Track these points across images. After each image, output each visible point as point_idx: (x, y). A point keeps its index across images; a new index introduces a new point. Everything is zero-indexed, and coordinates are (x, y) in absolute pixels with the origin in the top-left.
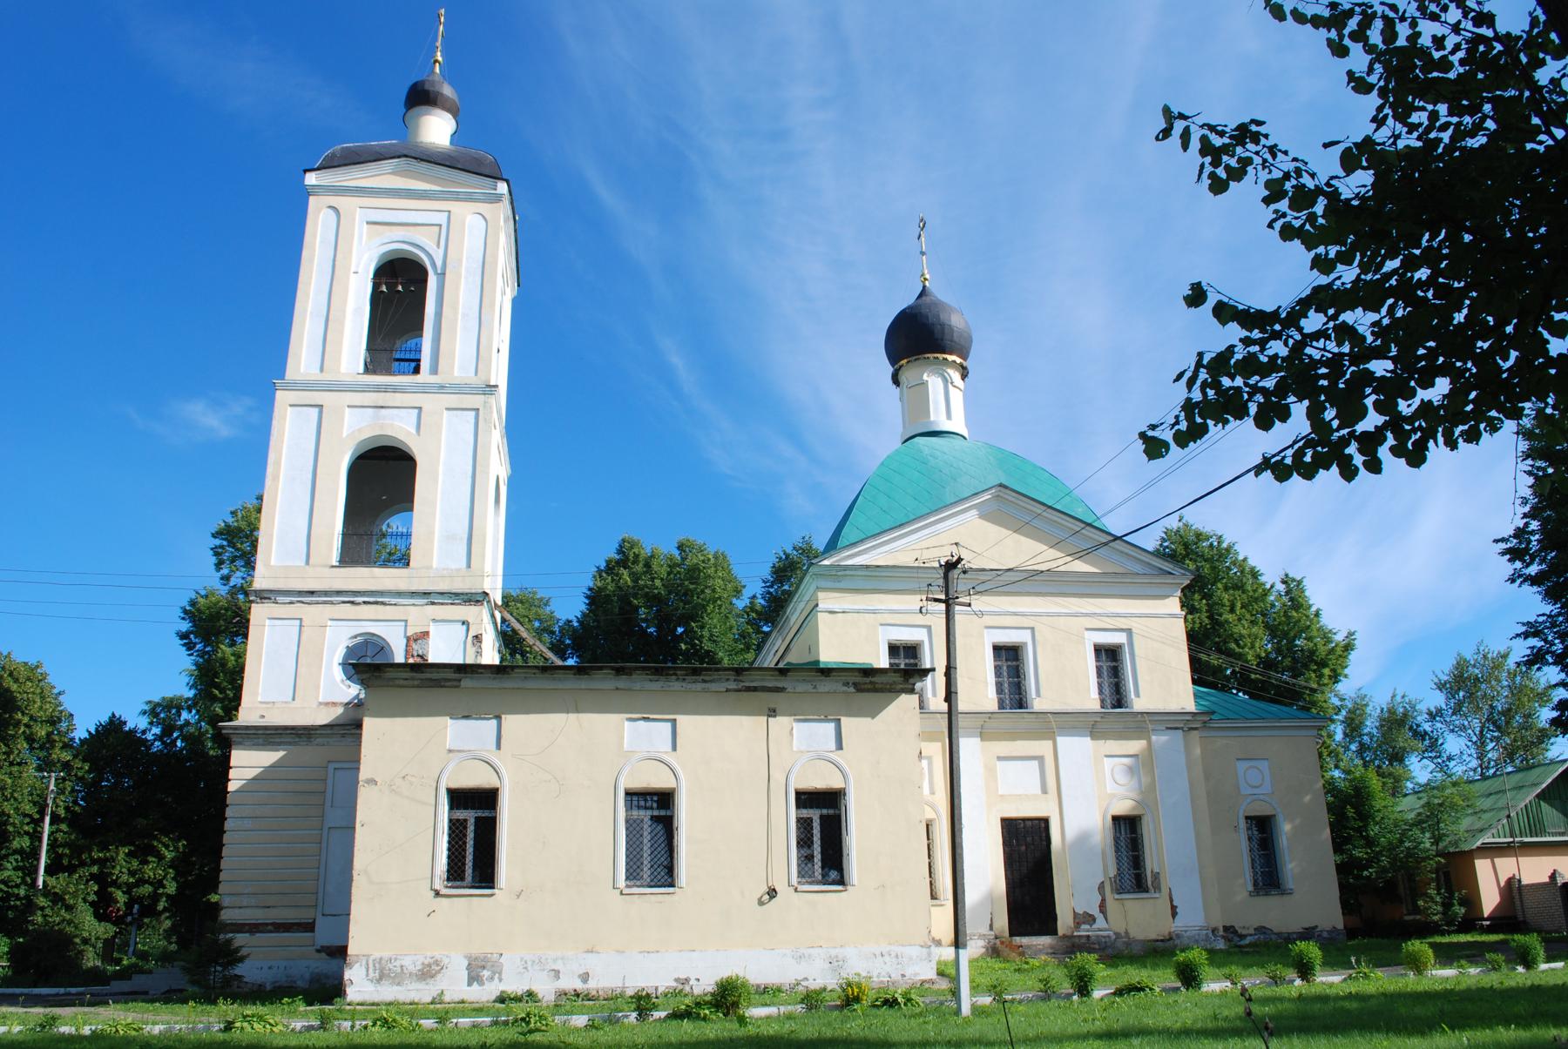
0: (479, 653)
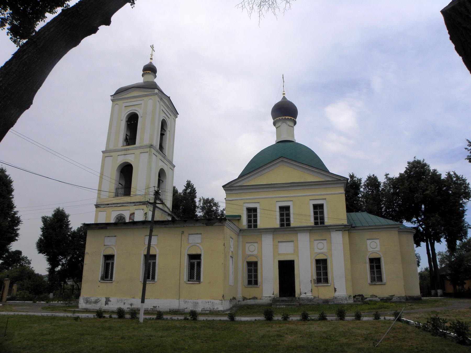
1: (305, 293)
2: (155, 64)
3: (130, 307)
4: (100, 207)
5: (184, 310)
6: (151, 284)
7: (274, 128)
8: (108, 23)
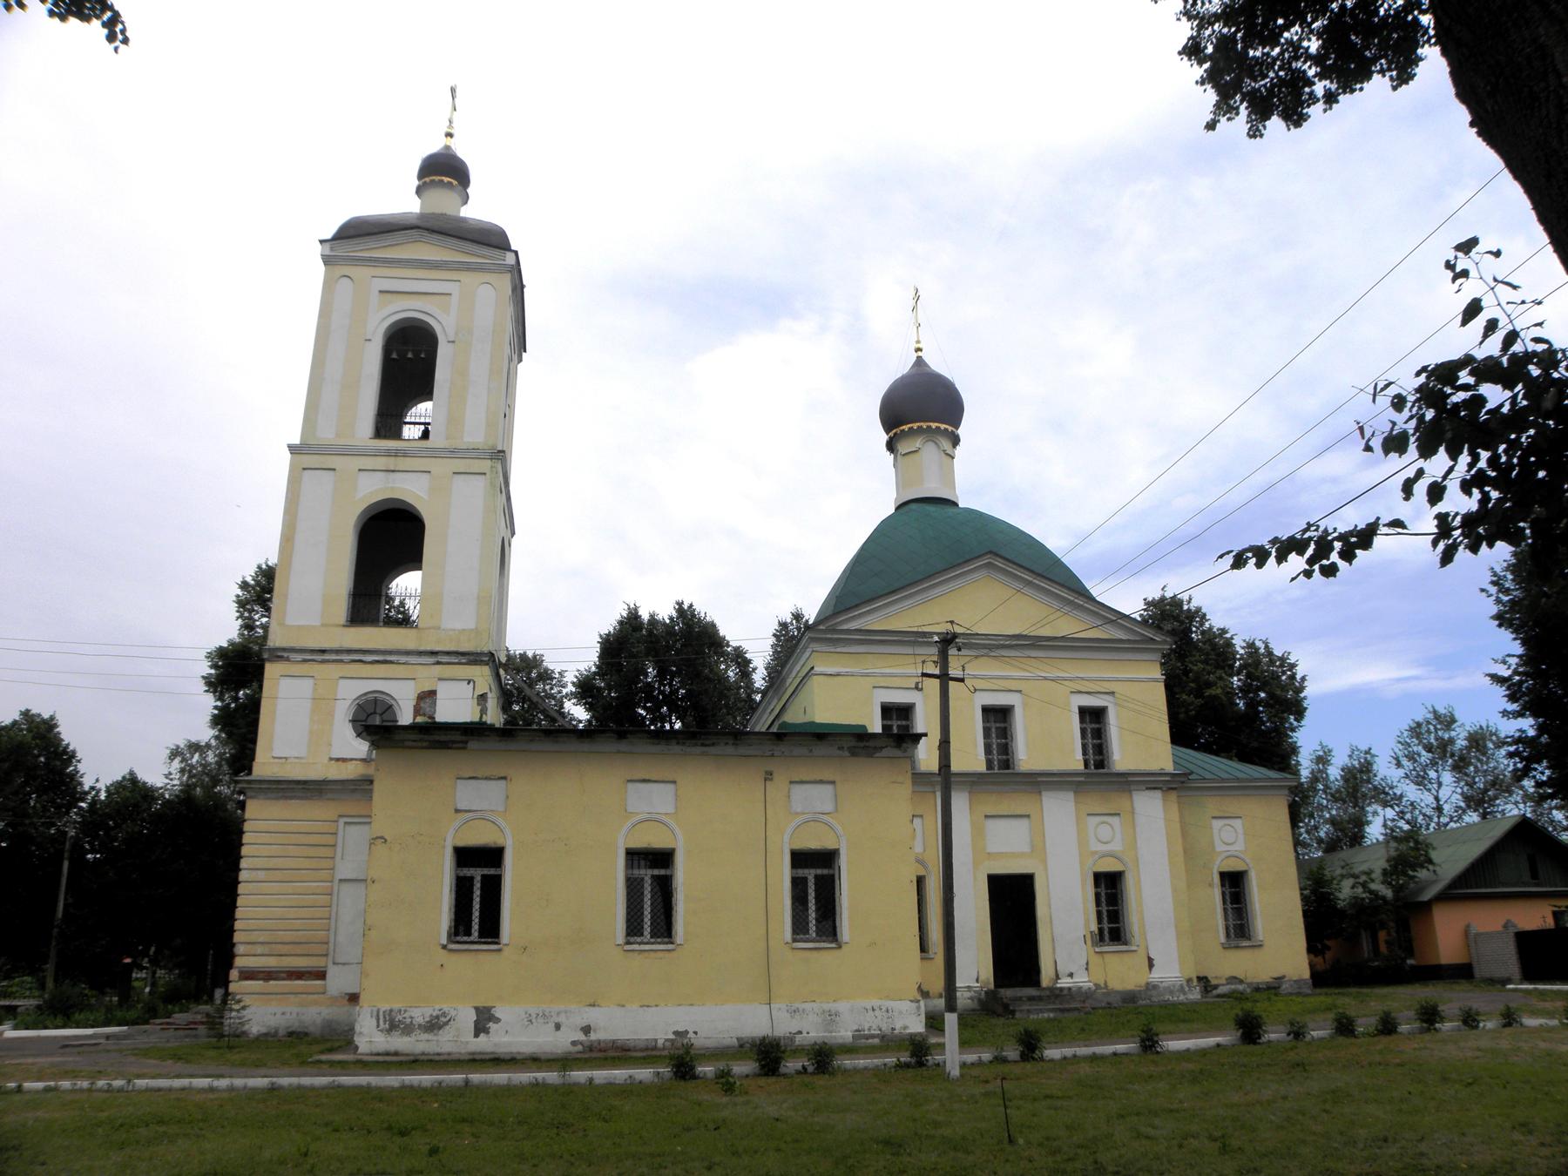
0: (483, 711)
1: (1071, 975)
2: (462, 151)
3: (582, 1037)
4: (288, 659)
5: (792, 1040)
6: (660, 954)
7: (890, 458)
8: (1472, 124)
